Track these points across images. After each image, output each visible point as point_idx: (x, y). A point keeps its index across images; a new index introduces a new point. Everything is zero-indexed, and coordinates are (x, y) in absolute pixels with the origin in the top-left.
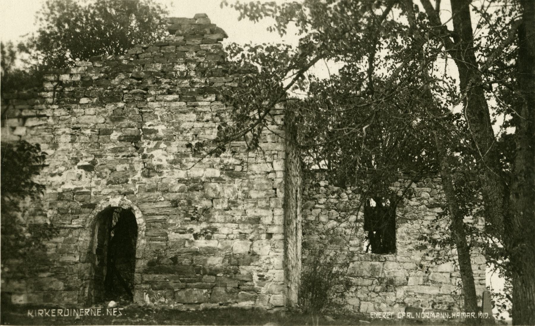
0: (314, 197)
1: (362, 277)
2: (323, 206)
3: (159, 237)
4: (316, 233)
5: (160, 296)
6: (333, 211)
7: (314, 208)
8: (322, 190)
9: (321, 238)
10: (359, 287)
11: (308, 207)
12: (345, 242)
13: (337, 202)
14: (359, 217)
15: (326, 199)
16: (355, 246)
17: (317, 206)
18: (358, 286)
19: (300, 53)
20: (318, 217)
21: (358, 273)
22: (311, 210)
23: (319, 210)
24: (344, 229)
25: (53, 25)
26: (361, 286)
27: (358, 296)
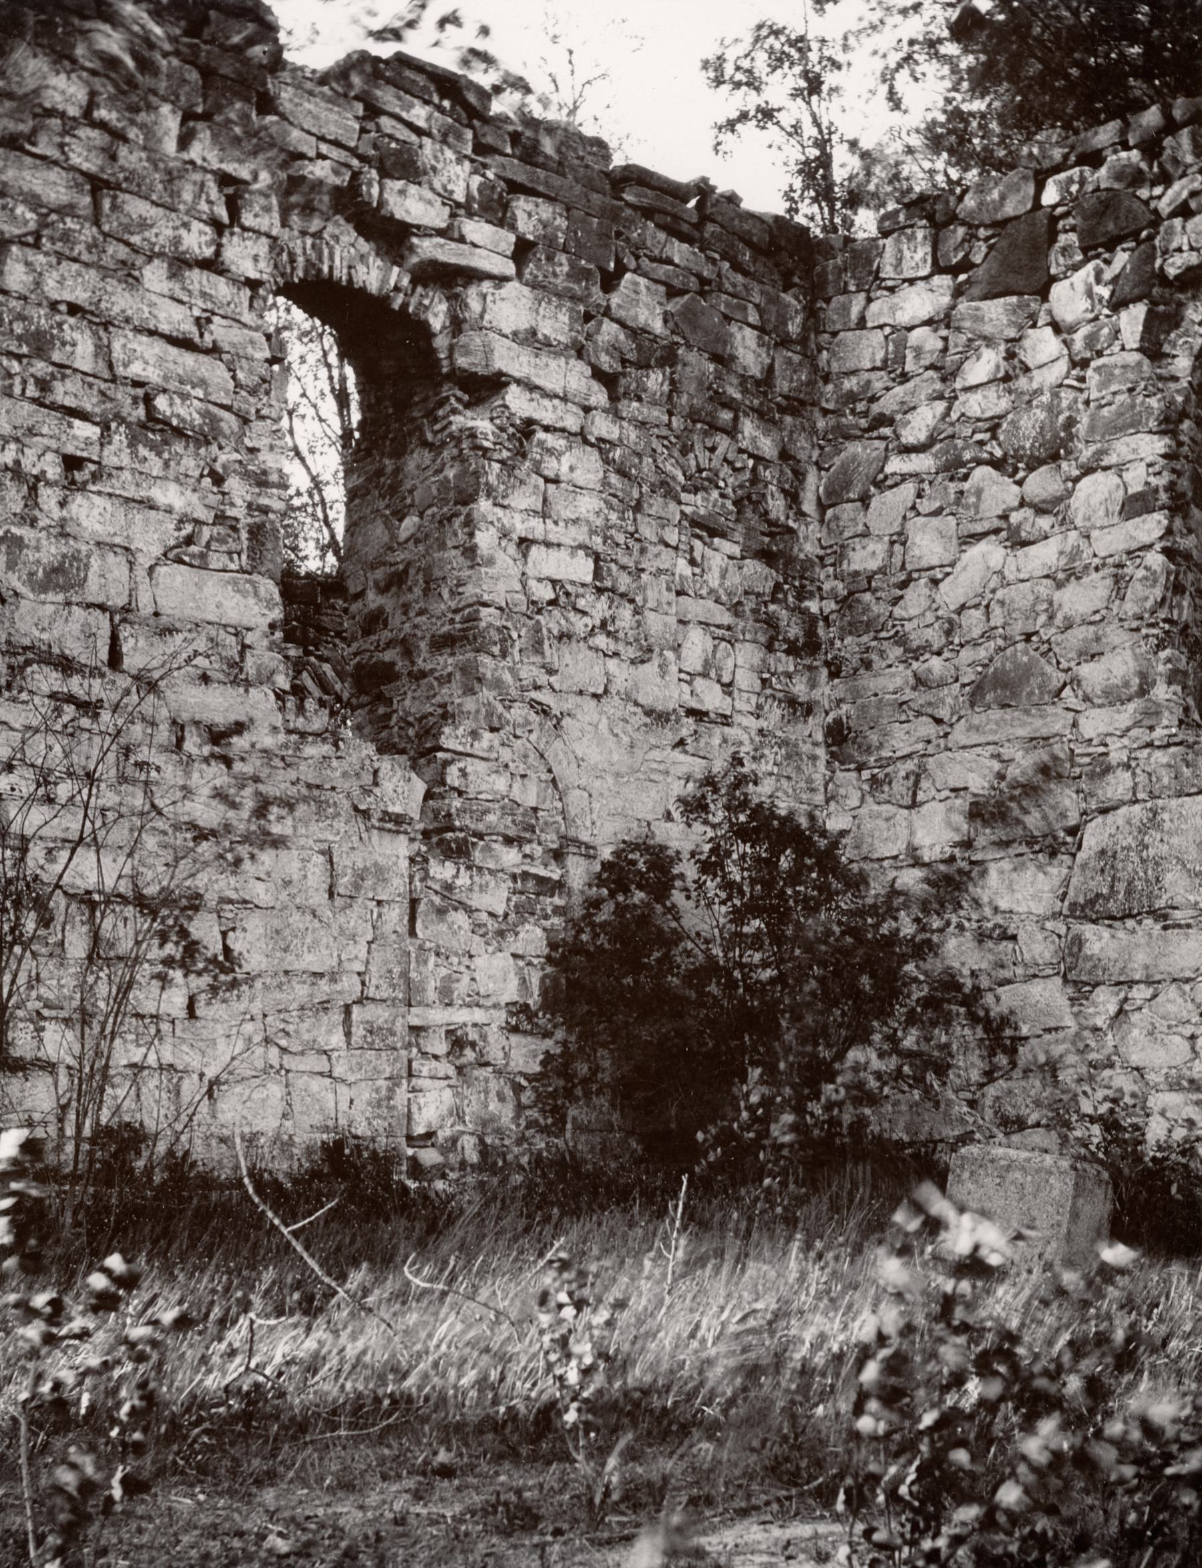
0: (876, 408)
1: (1160, 916)
2: (923, 463)
3: (327, 667)
4: (896, 652)
5: (441, 1172)
6: (982, 473)
7: (881, 483)
8: (918, 351)
9: (920, 682)
10: (1140, 993)
11: (847, 485)
12: (1057, 677)
13: (1004, 404)
14: (1136, 479)
15: (940, 406)
16: (1114, 697)
17: (896, 465)
18: (1131, 983)
19: (1179, 689)
20: (900, 538)
21: (1129, 892)
22: (865, 500)
23: (909, 488)
24: (1045, 588)
25: (404, 680)
26: (1149, 982)
27: (1135, 1059)
